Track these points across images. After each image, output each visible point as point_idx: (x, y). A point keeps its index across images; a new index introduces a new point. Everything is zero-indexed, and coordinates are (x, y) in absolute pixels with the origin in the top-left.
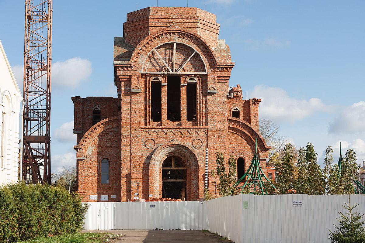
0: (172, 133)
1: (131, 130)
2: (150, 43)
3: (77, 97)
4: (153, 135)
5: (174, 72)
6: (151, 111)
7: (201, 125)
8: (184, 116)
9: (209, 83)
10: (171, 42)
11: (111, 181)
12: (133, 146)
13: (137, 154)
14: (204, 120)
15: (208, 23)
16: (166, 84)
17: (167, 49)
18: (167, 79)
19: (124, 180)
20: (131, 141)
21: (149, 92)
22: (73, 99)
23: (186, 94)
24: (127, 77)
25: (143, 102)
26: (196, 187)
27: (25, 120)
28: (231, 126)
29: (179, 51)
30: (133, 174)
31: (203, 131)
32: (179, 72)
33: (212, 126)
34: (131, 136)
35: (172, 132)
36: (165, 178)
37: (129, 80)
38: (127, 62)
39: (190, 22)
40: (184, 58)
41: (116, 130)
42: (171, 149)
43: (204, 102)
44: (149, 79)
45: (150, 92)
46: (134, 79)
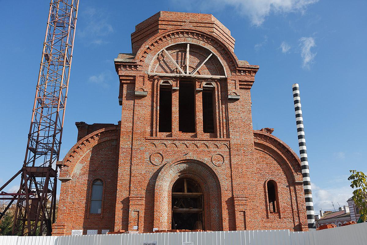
0: (185, 146)
1: (132, 141)
2: (160, 42)
3: (82, 123)
4: (161, 148)
5: (188, 75)
6: (158, 119)
7: (222, 137)
8: (200, 127)
9: (229, 87)
10: (184, 42)
11: (104, 210)
12: (135, 161)
13: (140, 171)
14: (225, 131)
15: (223, 33)
16: (178, 88)
17: (179, 51)
18: (178, 83)
19: (119, 206)
20: (131, 155)
21: (157, 97)
22: (77, 124)
23: (202, 101)
24: (130, 78)
25: (150, 108)
26: (218, 218)
27: (29, 150)
28: (257, 141)
29: (193, 54)
30: (132, 199)
31: (225, 144)
32: (194, 75)
33: (235, 138)
34: (132, 148)
35: (186, 145)
36: (176, 207)
37: (132, 82)
38: (131, 61)
39: (204, 26)
40: (199, 62)
41: (114, 143)
42: (184, 166)
43: (224, 111)
44: (158, 83)
45: (159, 97)
46: (138, 84)
